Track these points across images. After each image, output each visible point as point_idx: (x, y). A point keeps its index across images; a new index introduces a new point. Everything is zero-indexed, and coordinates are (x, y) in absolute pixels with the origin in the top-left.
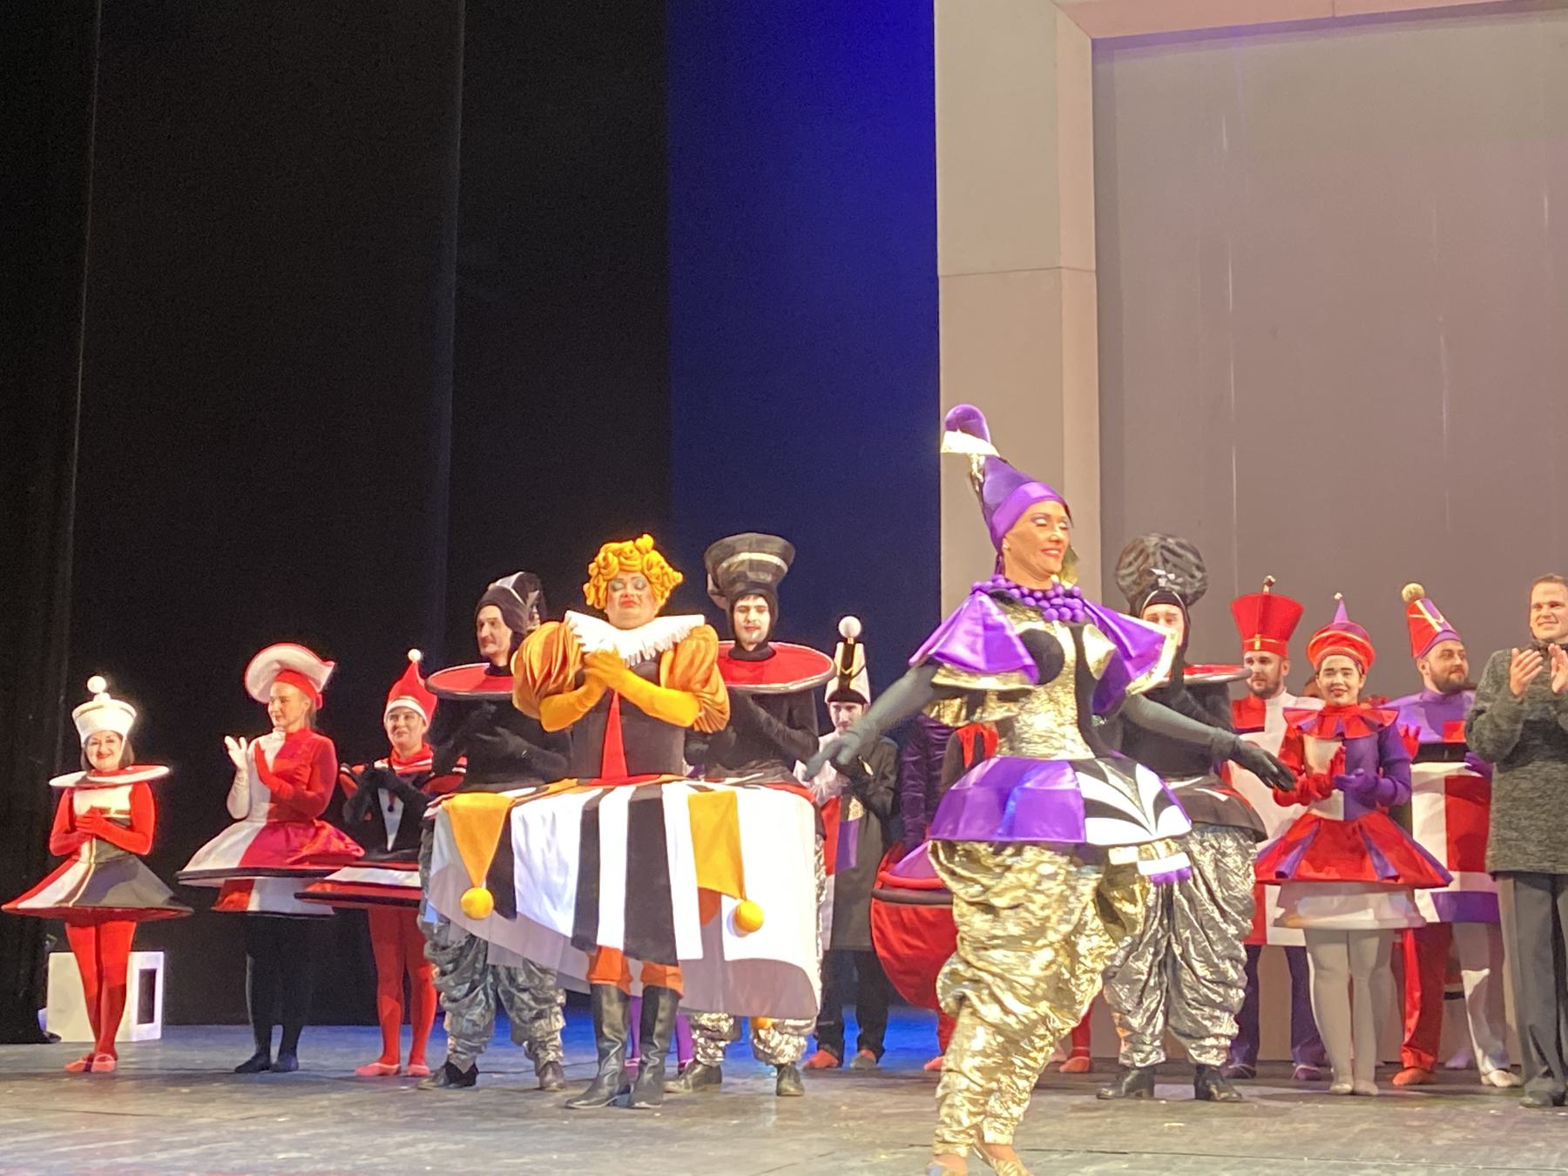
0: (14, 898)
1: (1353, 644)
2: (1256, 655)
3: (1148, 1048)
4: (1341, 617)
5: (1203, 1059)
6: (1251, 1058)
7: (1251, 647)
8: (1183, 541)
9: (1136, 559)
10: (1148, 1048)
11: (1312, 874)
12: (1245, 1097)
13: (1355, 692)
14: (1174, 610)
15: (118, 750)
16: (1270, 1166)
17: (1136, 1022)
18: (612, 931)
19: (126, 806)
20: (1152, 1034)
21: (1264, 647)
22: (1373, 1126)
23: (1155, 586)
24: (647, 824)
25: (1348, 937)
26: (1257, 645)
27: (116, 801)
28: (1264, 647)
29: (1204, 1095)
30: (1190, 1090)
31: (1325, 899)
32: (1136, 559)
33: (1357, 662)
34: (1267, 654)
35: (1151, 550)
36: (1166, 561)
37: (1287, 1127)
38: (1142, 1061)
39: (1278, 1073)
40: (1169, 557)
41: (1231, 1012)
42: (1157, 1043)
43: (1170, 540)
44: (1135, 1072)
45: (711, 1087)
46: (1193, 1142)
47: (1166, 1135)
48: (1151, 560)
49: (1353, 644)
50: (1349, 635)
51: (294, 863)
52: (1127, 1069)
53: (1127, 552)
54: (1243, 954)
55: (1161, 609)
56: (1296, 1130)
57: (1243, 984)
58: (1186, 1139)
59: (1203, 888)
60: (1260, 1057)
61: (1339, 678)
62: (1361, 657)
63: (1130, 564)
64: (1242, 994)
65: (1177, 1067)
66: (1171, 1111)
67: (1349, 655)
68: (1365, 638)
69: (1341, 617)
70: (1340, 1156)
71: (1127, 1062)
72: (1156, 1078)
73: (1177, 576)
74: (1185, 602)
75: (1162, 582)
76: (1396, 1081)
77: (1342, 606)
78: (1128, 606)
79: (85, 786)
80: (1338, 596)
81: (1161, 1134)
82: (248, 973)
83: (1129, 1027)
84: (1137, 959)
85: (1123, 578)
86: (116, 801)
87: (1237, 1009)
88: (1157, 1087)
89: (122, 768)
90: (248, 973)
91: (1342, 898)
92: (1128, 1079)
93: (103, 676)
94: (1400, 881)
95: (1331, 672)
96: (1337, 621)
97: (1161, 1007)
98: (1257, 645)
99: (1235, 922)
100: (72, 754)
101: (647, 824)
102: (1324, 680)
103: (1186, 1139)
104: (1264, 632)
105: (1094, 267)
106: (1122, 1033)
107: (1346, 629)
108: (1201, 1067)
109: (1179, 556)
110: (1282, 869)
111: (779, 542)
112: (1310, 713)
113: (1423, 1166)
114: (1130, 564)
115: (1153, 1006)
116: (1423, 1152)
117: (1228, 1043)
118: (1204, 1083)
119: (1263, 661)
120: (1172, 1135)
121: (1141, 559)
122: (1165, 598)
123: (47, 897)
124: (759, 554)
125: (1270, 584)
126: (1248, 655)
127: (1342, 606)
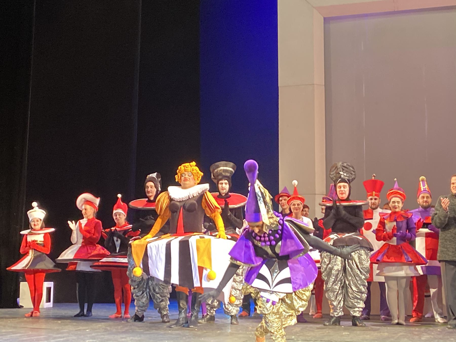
1: (401, 194)
4: (396, 186)
5: (355, 314)
6: (368, 314)
11: (388, 260)
12: (366, 325)
13: (400, 208)
14: (346, 184)
15: (40, 224)
17: (335, 303)
18: (175, 279)
19: (43, 240)
20: (340, 307)
23: (340, 177)
24: (185, 248)
25: (397, 278)
26: (374, 195)
27: (39, 238)
28: (376, 195)
29: (355, 325)
30: (351, 323)
31: (391, 267)
33: (402, 199)
34: (376, 197)
35: (339, 167)
36: (343, 170)
37: (379, 334)
38: (337, 315)
39: (376, 318)
40: (344, 168)
41: (363, 301)
42: (341, 310)
44: (335, 318)
45: (212, 322)
47: (344, 336)
48: (339, 170)
49: (401, 194)
50: (399, 191)
52: (332, 317)
53: (332, 167)
54: (367, 284)
55: (342, 184)
59: (355, 265)
60: (371, 314)
62: (402, 198)
64: (366, 295)
65: (347, 316)
66: (345, 329)
67: (399, 197)
68: (403, 192)
69: (396, 186)
71: (332, 315)
75: (342, 176)
76: (410, 321)
77: (396, 182)
79: (31, 234)
80: (395, 179)
83: (333, 305)
86: (39, 238)
87: (365, 300)
89: (41, 229)
91: (396, 267)
92: (333, 320)
94: (413, 262)
95: (394, 202)
96: (395, 187)
97: (343, 299)
99: (364, 275)
100: (27, 225)
101: (185, 248)
102: (391, 204)
105: (324, 84)
106: (331, 307)
107: (398, 190)
108: (354, 317)
109: (347, 168)
110: (378, 258)
111: (232, 164)
112: (387, 214)
115: (340, 299)
117: (362, 310)
118: (354, 321)
119: (375, 199)
122: (343, 181)
123: (21, 266)
124: (226, 168)
125: (374, 176)
127: (396, 182)
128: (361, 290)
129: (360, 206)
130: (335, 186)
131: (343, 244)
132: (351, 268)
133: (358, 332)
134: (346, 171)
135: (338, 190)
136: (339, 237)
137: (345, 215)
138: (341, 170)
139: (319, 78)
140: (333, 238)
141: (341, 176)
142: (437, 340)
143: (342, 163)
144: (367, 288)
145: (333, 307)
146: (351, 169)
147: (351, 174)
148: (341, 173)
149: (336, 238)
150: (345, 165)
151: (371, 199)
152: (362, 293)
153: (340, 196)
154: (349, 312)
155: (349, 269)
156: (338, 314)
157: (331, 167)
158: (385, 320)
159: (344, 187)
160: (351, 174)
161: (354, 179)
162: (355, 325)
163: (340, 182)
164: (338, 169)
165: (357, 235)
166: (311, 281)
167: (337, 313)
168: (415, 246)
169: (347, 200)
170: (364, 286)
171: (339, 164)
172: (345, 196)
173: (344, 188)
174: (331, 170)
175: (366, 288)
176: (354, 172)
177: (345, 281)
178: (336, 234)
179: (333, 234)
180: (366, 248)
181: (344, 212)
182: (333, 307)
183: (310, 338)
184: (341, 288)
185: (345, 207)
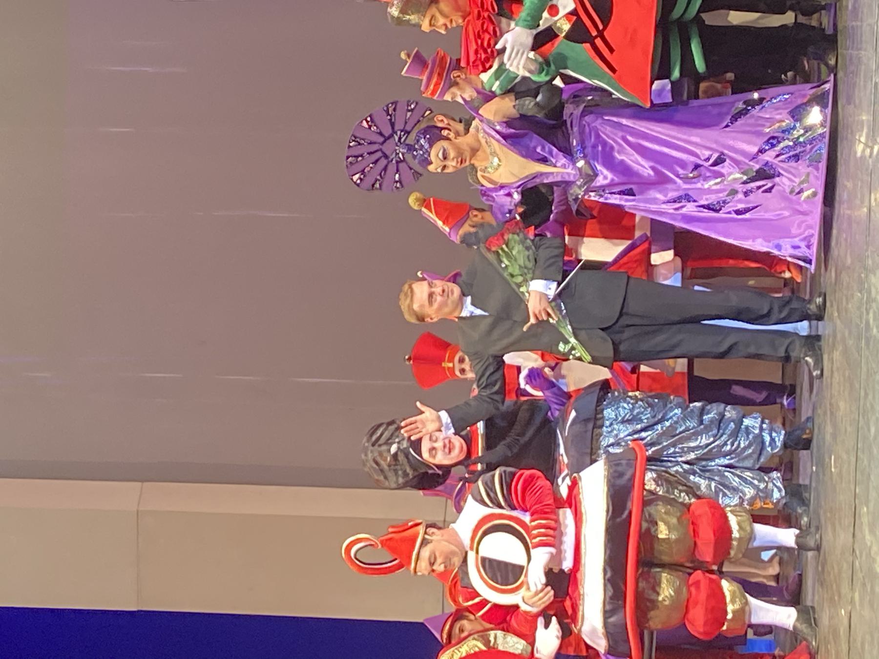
0: (752, 596)
2: (458, 367)
10: (770, 485)
12: (810, 414)
16: (866, 394)
17: (749, 492)
20: (759, 481)
21: (451, 360)
22: (835, 307)
26: (451, 365)
28: (451, 360)
29: (807, 444)
30: (804, 453)
34: (457, 359)
38: (780, 490)
46: (848, 452)
47: (841, 471)
51: (764, 186)
54: (698, 404)
56: (838, 369)
58: (845, 457)
59: (644, 434)
60: (780, 382)
61: (439, 445)
65: (786, 465)
66: (821, 464)
70: (859, 338)
76: (799, 280)
81: (840, 474)
84: (699, 488)
97: (738, 472)
98: (451, 365)
103: (845, 457)
108: (785, 446)
113: (867, 276)
115: (736, 479)
116: (856, 275)
118: (799, 442)
119: (462, 361)
128: (712, 421)
136: (566, 472)
137: (509, 447)
139: (123, 496)
144: (710, 403)
145: (758, 500)
151: (463, 371)
152: (722, 416)
158: (791, 470)
162: (807, 444)
166: (740, 540)
170: (702, 412)
178: (560, 480)
180: (600, 401)
184: (707, 474)
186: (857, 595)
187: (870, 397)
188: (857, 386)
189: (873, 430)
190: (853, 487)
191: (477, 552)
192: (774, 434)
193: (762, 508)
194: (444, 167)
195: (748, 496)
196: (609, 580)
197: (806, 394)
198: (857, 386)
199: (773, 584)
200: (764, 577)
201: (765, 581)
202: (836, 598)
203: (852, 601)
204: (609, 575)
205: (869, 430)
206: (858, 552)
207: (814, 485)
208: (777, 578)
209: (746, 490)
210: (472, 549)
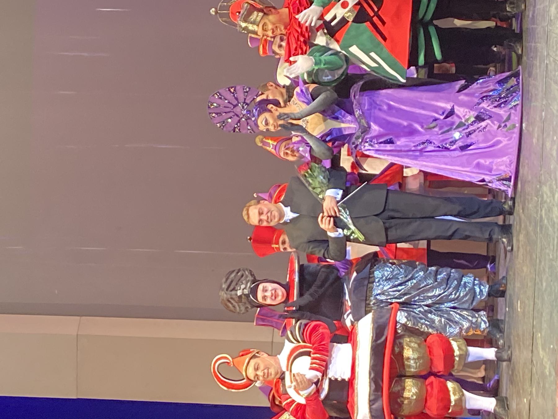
3: (479, 320)
5: (485, 294)
7: (278, 249)
8: (224, 280)
9: (232, 304)
10: (479, 320)
14: (261, 287)
16: (540, 261)
17: (466, 325)
20: (472, 317)
21: (277, 243)
23: (247, 296)
28: (277, 243)
29: (502, 294)
30: (500, 300)
32: (232, 304)
36: (234, 289)
40: (231, 288)
43: (224, 286)
48: (234, 297)
53: (228, 307)
54: (434, 268)
55: (260, 294)
57: (449, 269)
58: (527, 302)
60: (486, 254)
63: (234, 307)
64: (453, 270)
65: (490, 308)
66: (512, 306)
72: (495, 318)
73: (242, 284)
74: (256, 282)
75: (246, 291)
77: (260, 195)
78: (255, 308)
82: (62, 53)
83: (468, 330)
85: (241, 310)
88: (499, 318)
90: (62, 53)
93: (418, 389)
104: (270, 243)
105: (78, 318)
108: (489, 294)
109: (232, 282)
113: (541, 187)
114: (234, 307)
115: (458, 316)
118: (498, 292)
119: (284, 243)
120: (524, 308)
121: (232, 301)
122: (254, 291)
126: (282, 250)
127: (260, 195)
128: (442, 279)
129: (301, 267)
130: (261, 306)
131: (364, 305)
132: (405, 294)
133: (518, 285)
134: (237, 284)
135: (269, 302)
136: (349, 311)
138: (233, 292)
139: (68, 326)
140: (351, 321)
141: (245, 295)
142: (554, 86)
143: (223, 290)
145: (471, 330)
146: (233, 275)
147: (242, 276)
148: (239, 293)
149: (351, 316)
150: (224, 286)
153: (280, 299)
154: (481, 301)
155: (405, 297)
156: (484, 321)
157: (226, 313)
159: (265, 290)
160: (242, 276)
161: (251, 272)
162: (502, 294)
163: (256, 297)
164: (232, 298)
165: (349, 279)
167: (483, 323)
168: (374, 175)
169: (288, 288)
170: (437, 273)
171: (224, 295)
172: (281, 291)
173: (266, 291)
174: (231, 311)
175: (440, 270)
176: (239, 271)
177: (427, 306)
178: (345, 316)
179: (344, 320)
181: (307, 298)
182: (471, 330)
183: (526, 371)
185: (301, 294)
186: (534, 389)
187: (543, 263)
188: (534, 257)
189: (544, 284)
190: (531, 321)
191: (291, 371)
192: (482, 287)
193: (474, 334)
194: (260, 220)
195: (465, 327)
196: (372, 379)
197: (502, 261)
198: (534, 257)
199: (481, 382)
200: (475, 378)
201: (475, 381)
202: (521, 391)
203: (531, 393)
204: (372, 375)
205: (542, 285)
206: (535, 362)
207: (507, 319)
208: (483, 379)
209: (464, 323)
210: (287, 370)
